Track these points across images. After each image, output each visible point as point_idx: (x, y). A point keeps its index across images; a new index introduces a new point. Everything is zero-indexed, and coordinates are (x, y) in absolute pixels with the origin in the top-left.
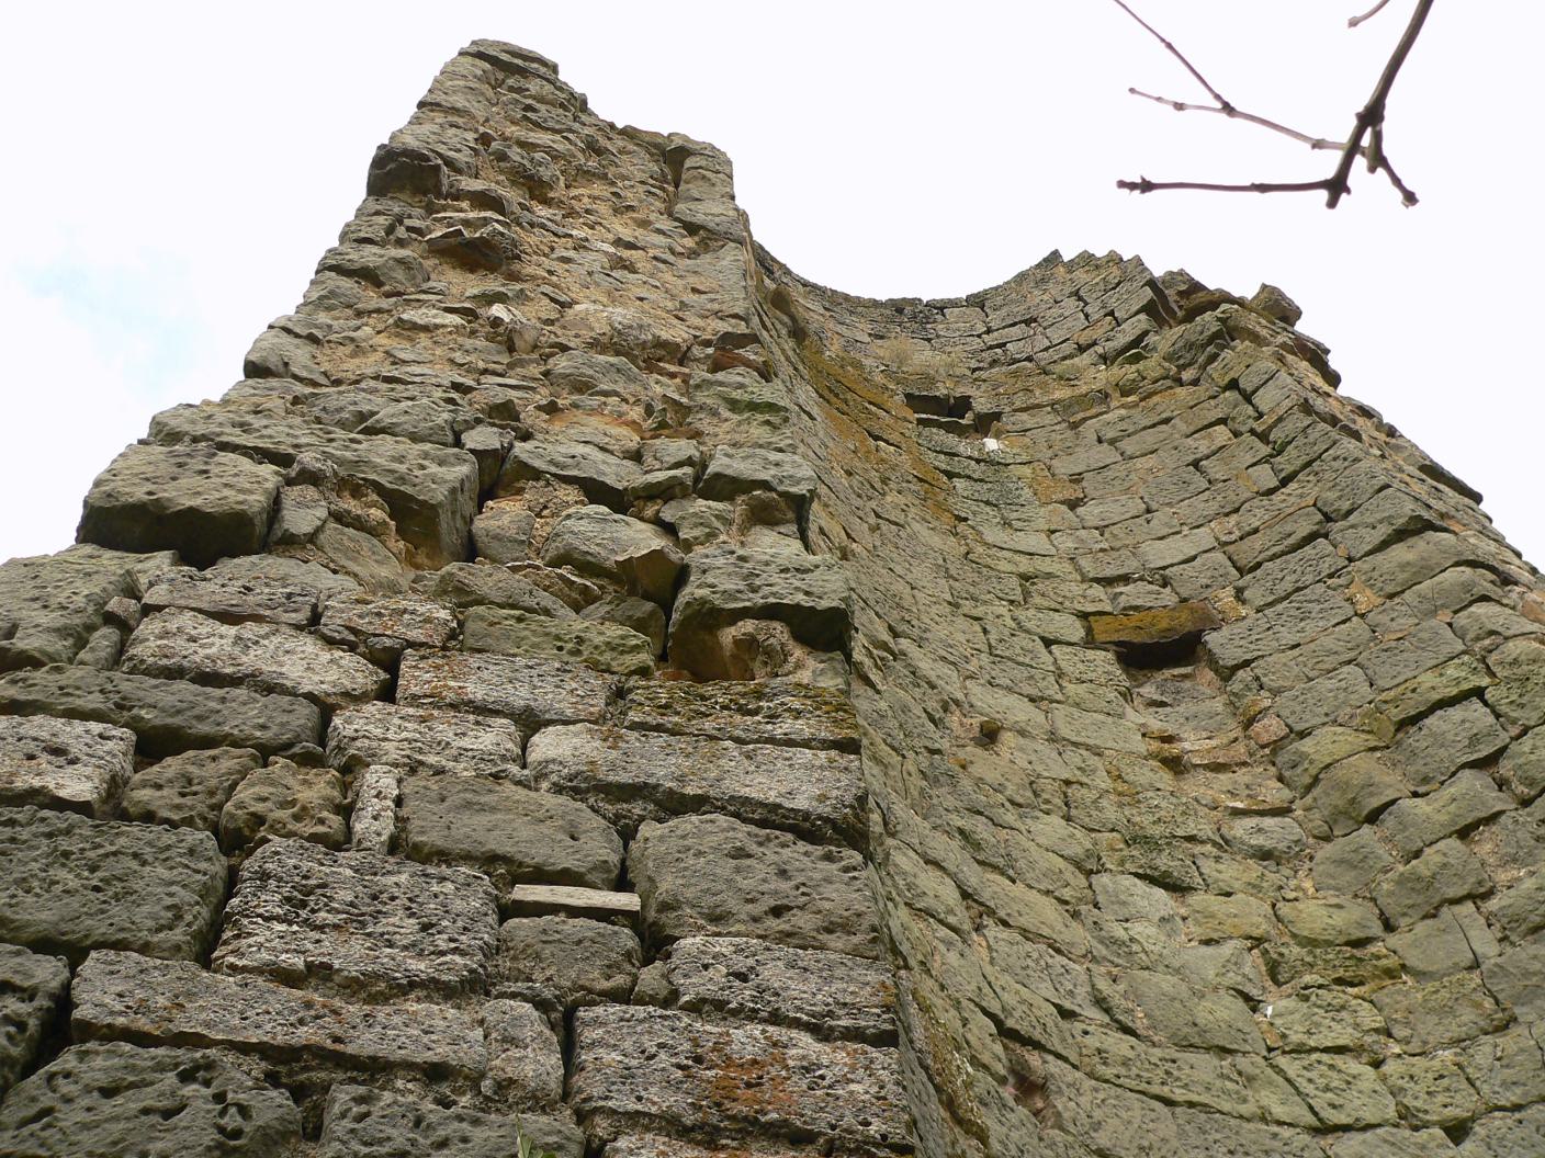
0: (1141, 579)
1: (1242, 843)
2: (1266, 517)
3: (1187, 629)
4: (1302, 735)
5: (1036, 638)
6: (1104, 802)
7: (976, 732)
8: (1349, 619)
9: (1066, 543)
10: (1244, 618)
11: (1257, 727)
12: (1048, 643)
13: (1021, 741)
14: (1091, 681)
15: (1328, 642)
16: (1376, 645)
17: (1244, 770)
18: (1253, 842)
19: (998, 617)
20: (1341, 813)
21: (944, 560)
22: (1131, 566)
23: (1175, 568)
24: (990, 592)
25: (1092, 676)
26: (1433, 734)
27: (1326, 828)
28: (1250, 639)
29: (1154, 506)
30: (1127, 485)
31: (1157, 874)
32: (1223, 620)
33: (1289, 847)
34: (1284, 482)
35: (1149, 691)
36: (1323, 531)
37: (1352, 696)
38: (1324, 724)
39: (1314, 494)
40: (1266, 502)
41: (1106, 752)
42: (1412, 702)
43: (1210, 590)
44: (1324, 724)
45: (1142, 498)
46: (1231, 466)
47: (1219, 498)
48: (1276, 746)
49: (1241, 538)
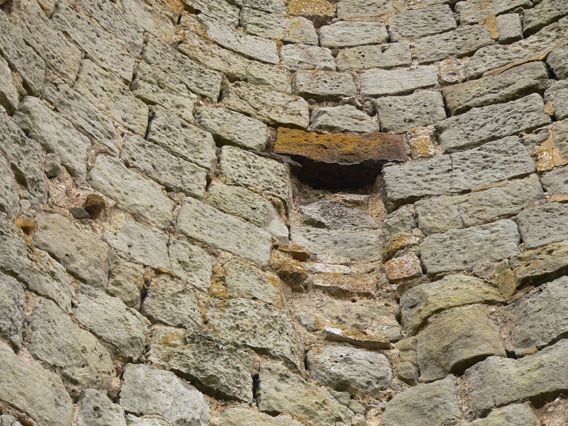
0: (351, 103)
1: (322, 369)
2: (494, 65)
3: (370, 157)
4: (435, 277)
5: (209, 135)
6: (185, 298)
7: (80, 204)
8: (527, 175)
9: (292, 54)
10: (431, 156)
11: (394, 261)
12: (220, 141)
13: (132, 223)
14: (246, 186)
15: (497, 193)
16: (541, 204)
17: (365, 300)
18: (333, 370)
19: (178, 107)
20: (432, 359)
21: (146, 42)
22: (346, 87)
23: (388, 98)
24: (181, 82)
25: (250, 181)
26: (549, 297)
27: (413, 370)
28: (427, 177)
29: (396, 36)
30: (380, 12)
31: (201, 376)
32: (410, 155)
33: (369, 383)
34: (527, 34)
35: (313, 210)
36: (541, 87)
37: (497, 249)
38: (458, 271)
39: (549, 49)
40: (501, 50)
41: (223, 254)
42: (542, 263)
43: (412, 125)
44: (458, 271)
45: (387, 27)
46: (485, 10)
47: (460, 39)
48: (405, 283)
49: (464, 81)
